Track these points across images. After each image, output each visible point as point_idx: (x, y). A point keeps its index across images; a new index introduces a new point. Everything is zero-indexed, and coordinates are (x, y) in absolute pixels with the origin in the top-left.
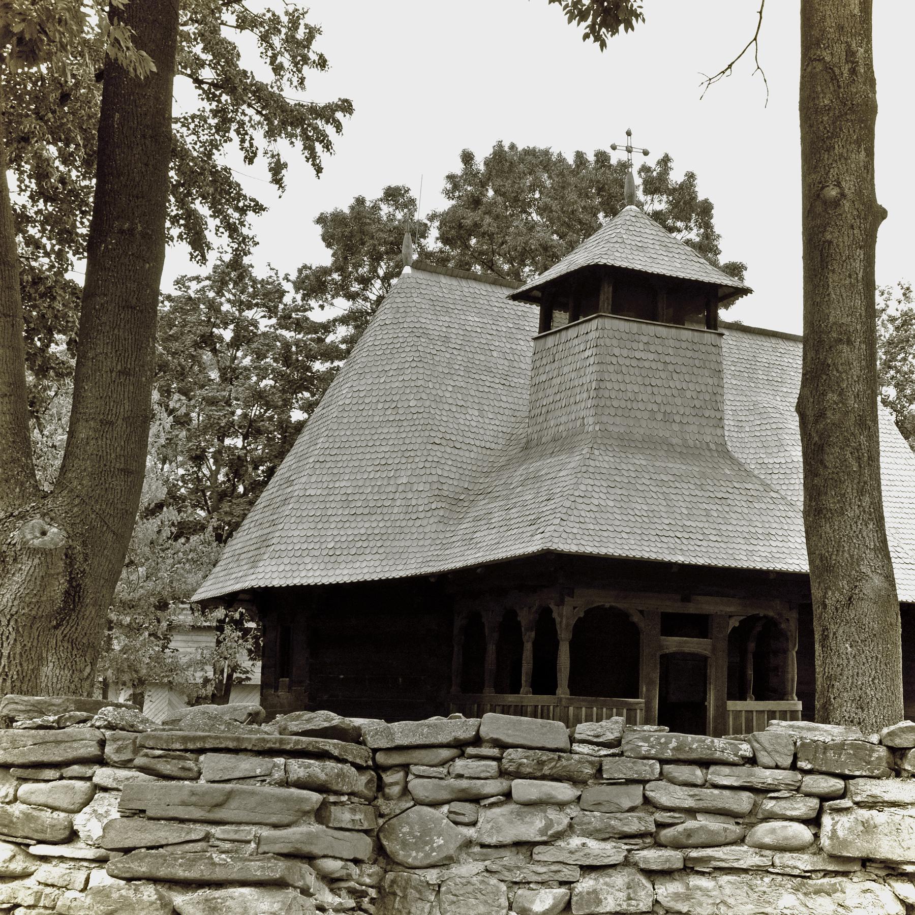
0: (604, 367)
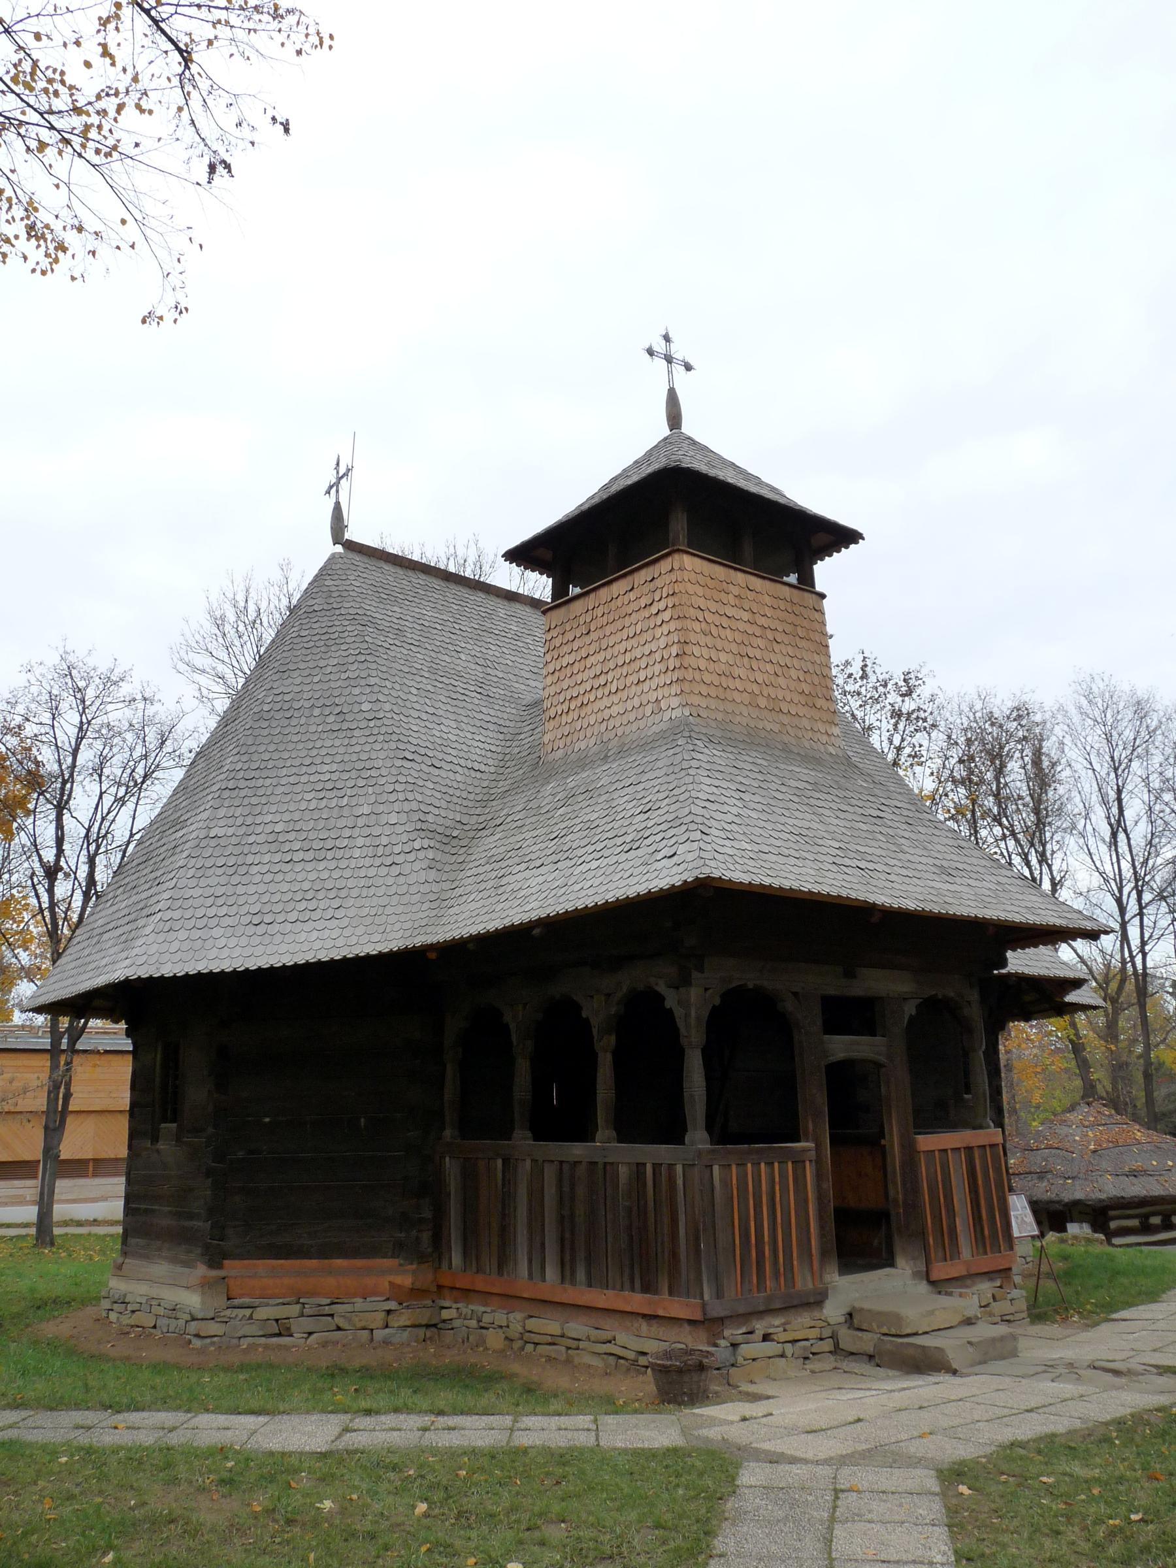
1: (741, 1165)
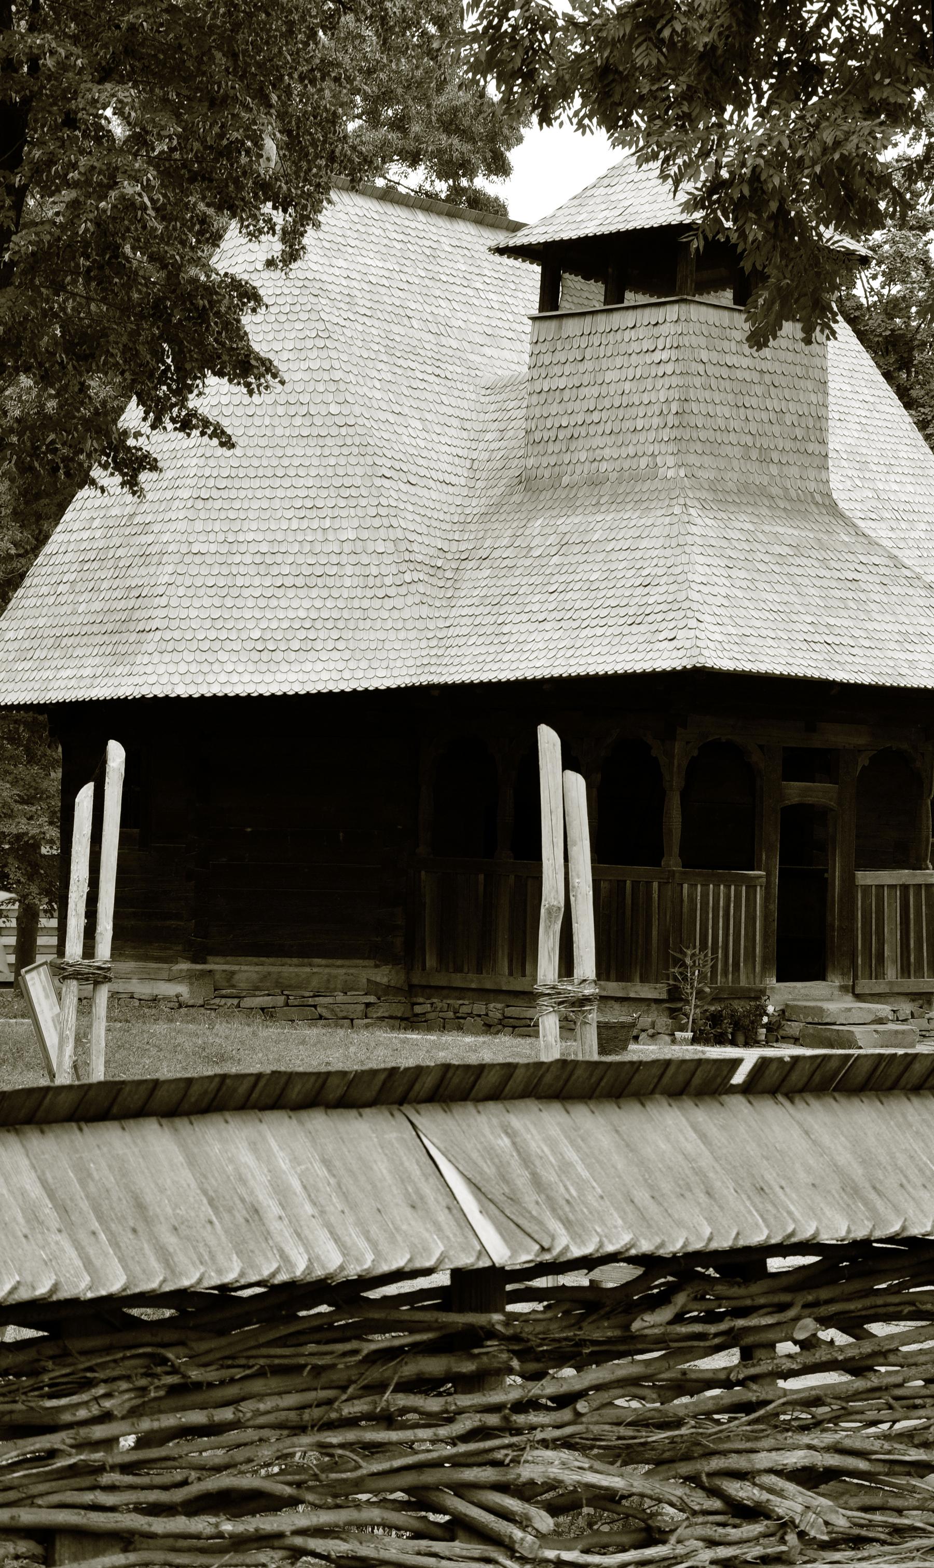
0: (689, 380)
1: (705, 885)
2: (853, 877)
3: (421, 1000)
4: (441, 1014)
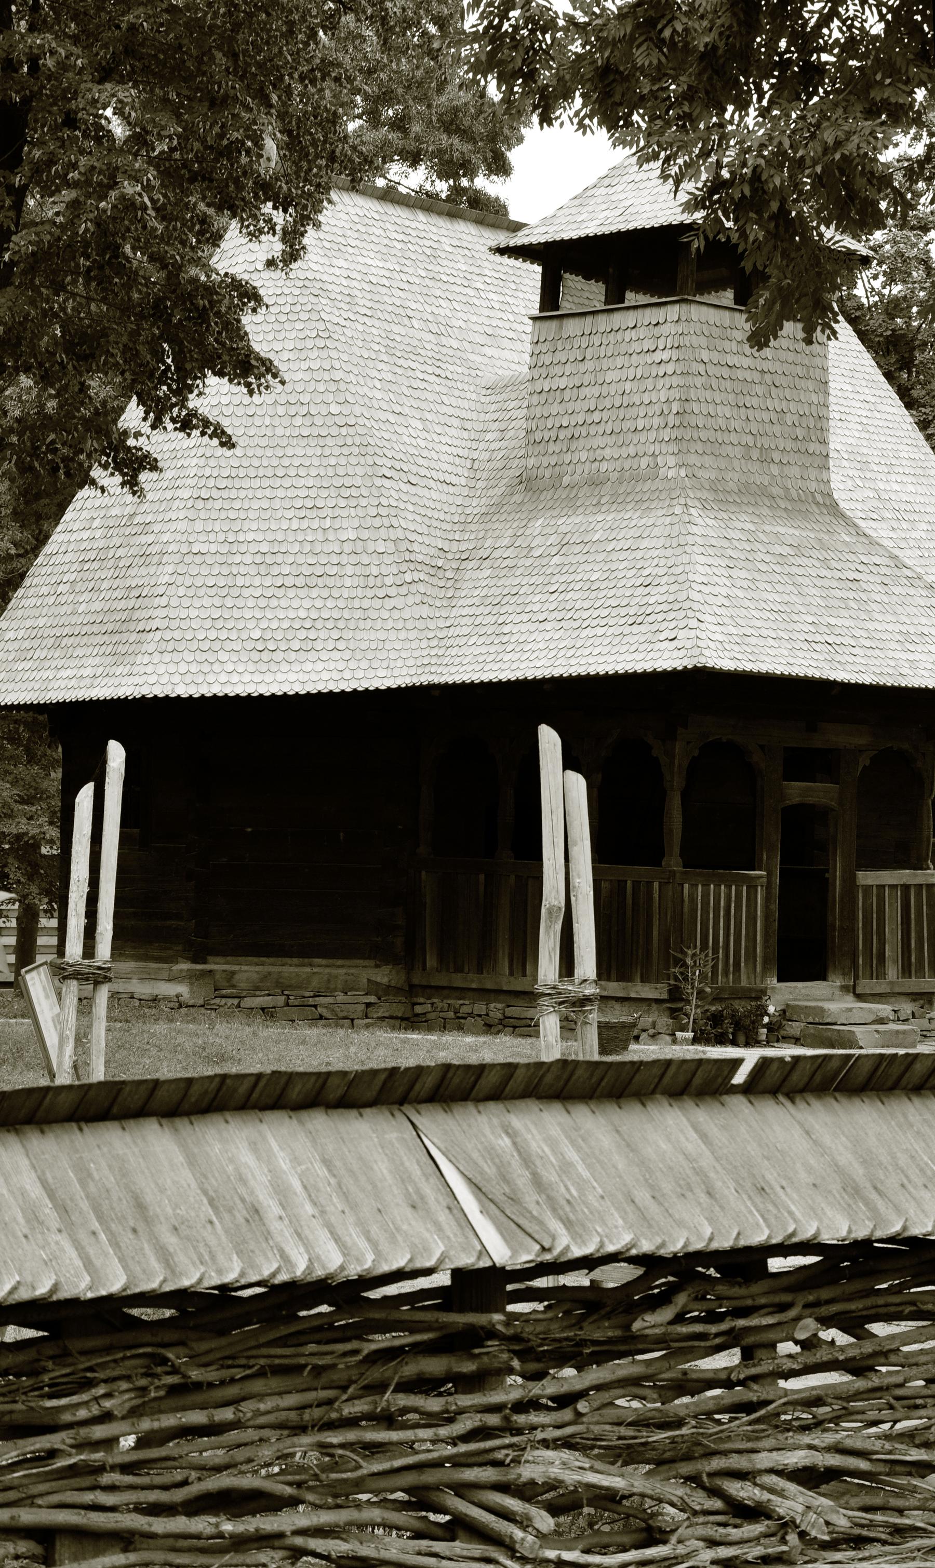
0: (690, 380)
1: (706, 885)
2: (854, 877)
3: (422, 1000)
4: (442, 1014)
